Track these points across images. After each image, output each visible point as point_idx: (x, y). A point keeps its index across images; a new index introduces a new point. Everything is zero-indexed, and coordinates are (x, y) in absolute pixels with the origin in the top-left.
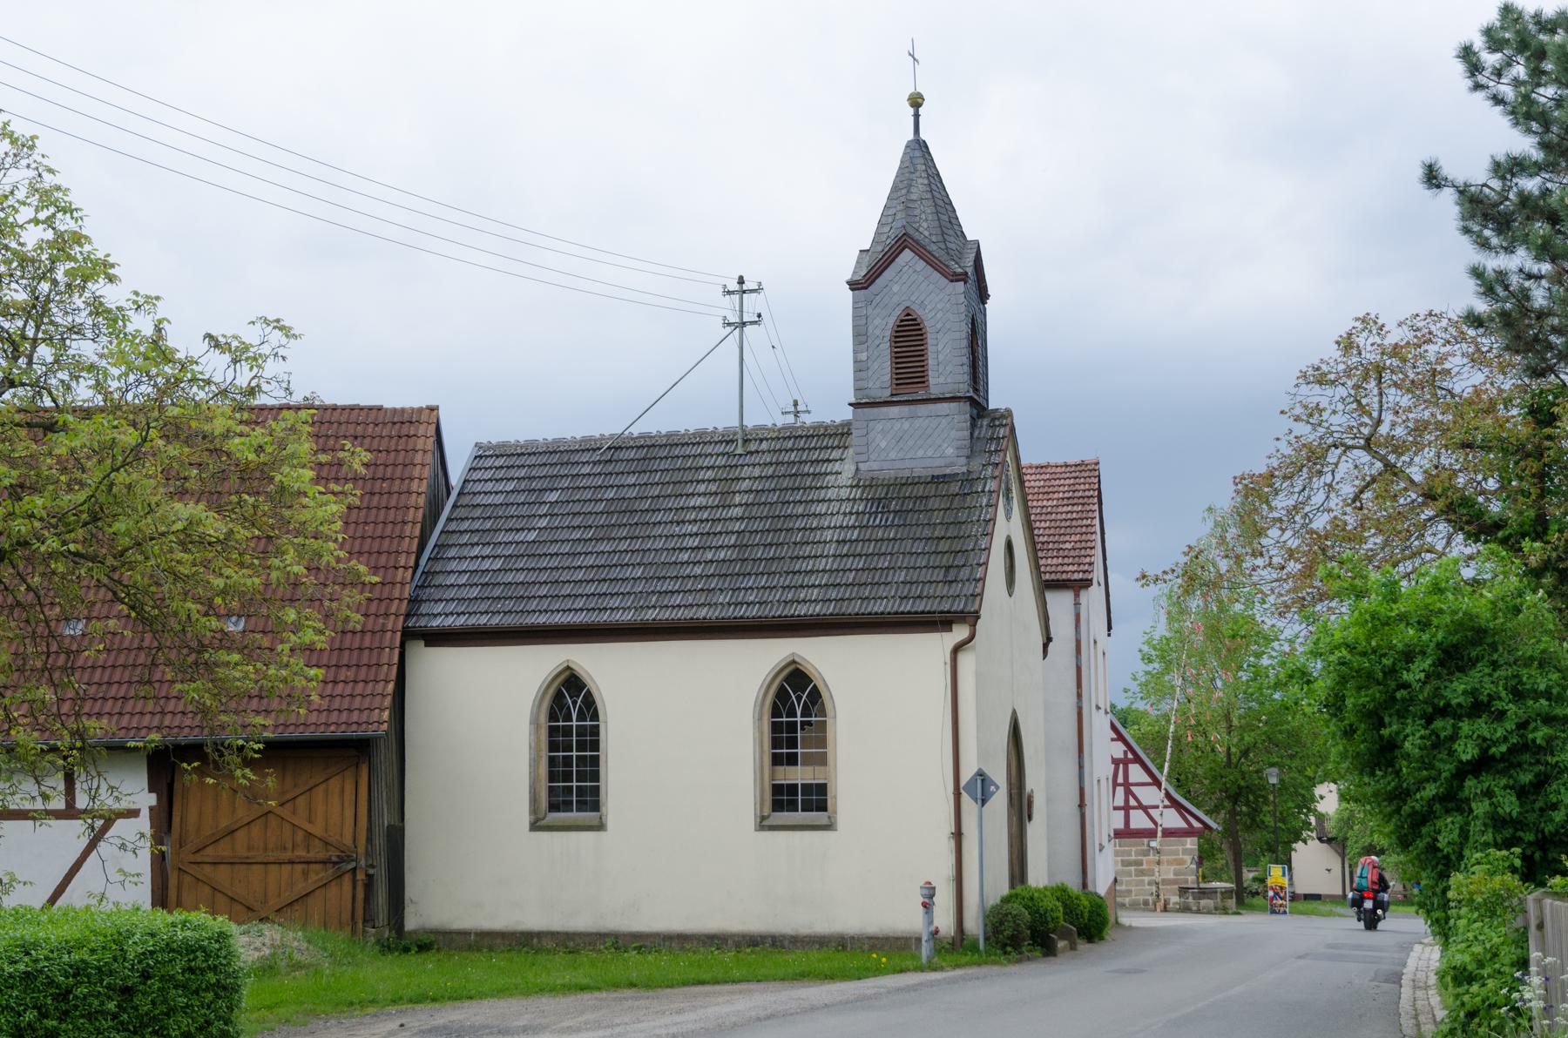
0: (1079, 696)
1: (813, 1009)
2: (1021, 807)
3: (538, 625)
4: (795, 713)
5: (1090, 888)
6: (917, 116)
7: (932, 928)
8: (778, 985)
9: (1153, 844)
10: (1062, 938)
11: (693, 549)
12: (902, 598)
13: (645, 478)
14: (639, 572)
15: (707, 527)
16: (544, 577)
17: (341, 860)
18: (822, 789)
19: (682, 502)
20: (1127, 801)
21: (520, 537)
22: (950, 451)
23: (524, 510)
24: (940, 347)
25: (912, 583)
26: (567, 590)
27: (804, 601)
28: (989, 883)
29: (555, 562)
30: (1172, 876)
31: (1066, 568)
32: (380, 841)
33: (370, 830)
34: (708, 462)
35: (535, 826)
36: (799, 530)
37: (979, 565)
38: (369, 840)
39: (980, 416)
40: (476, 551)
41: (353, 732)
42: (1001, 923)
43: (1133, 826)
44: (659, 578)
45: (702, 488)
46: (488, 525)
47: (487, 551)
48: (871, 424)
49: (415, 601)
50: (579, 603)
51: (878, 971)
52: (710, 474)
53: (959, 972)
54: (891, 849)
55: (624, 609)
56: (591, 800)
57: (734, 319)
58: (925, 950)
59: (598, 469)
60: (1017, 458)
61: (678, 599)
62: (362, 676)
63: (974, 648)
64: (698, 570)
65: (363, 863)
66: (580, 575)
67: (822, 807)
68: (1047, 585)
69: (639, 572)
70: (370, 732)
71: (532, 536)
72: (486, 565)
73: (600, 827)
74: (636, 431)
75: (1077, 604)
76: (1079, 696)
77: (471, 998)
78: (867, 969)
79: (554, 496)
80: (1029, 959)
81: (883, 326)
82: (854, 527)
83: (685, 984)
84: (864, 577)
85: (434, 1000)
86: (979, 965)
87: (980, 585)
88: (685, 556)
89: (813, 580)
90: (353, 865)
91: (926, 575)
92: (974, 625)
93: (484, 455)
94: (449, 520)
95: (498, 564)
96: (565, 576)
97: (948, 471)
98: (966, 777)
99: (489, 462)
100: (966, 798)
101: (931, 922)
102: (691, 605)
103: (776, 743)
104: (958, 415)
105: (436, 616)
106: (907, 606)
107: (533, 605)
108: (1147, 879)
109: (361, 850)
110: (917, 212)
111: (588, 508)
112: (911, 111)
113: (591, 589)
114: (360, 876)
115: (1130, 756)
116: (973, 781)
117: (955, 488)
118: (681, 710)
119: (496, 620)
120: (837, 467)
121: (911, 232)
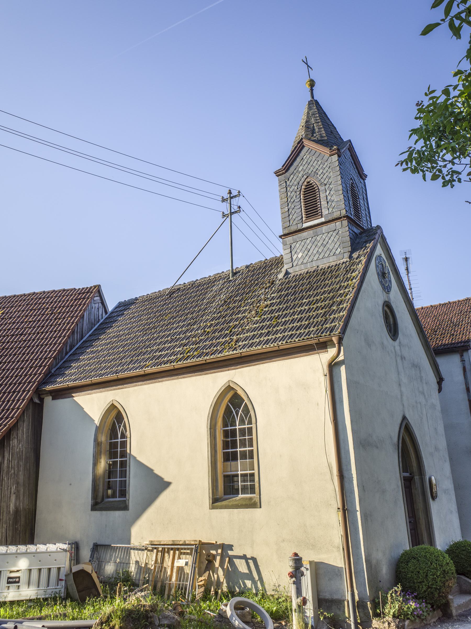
74: (187, 279)
104: (343, 228)
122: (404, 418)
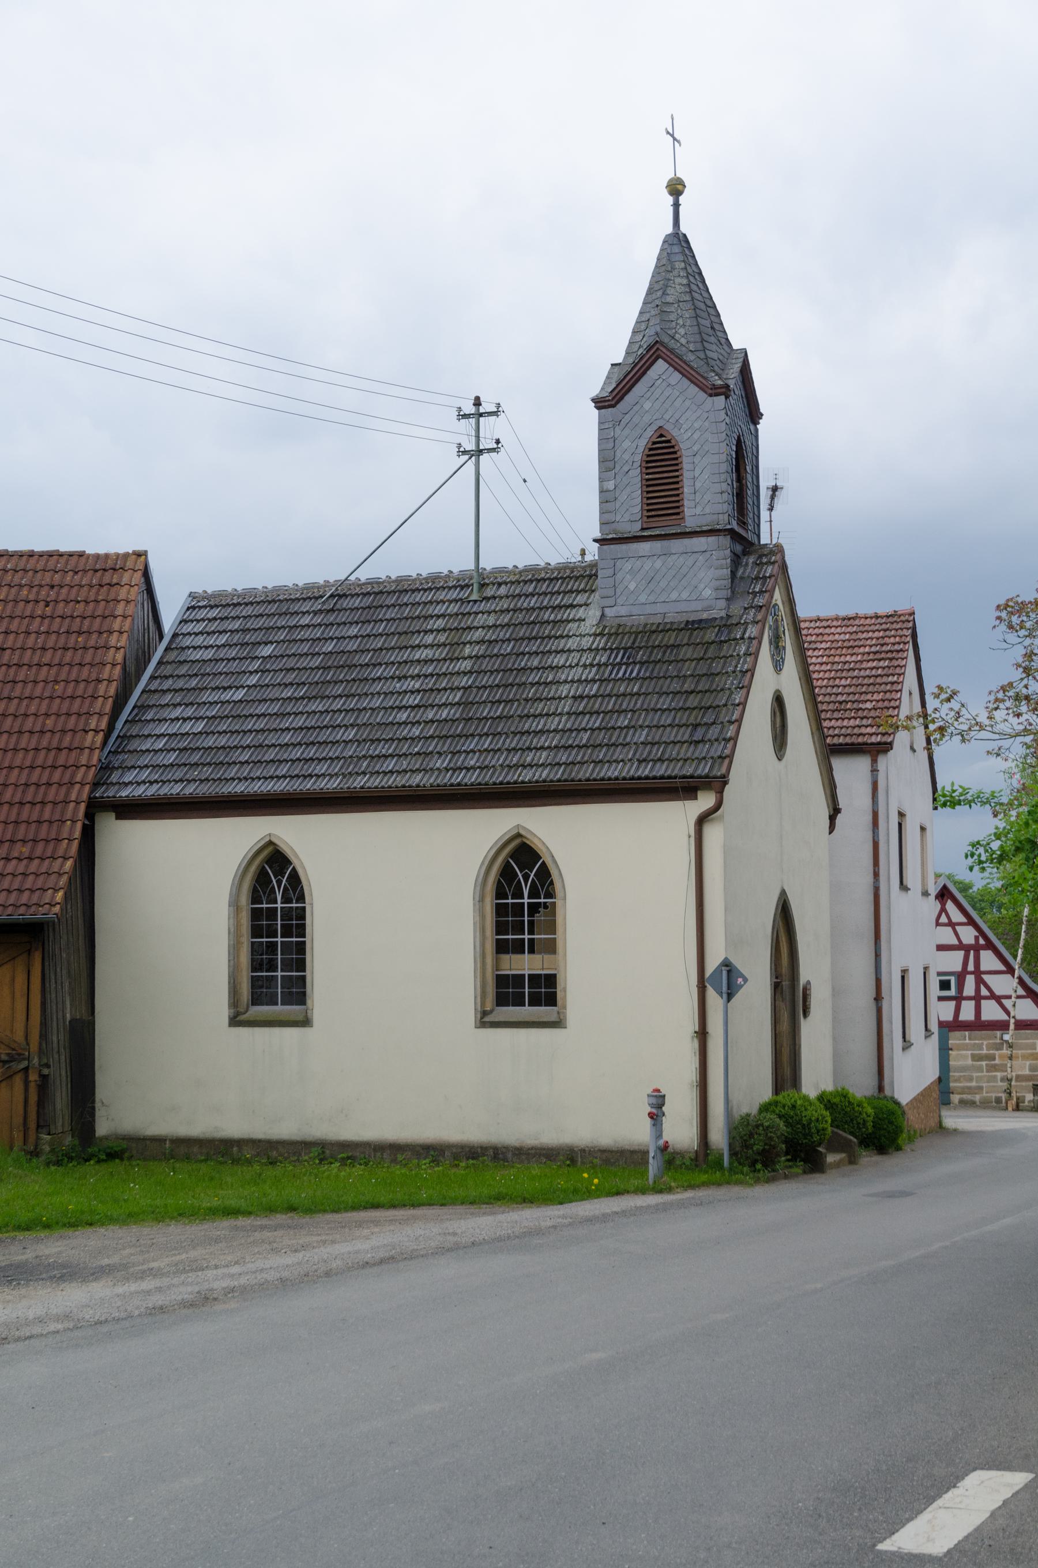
0: (876, 875)
1: (411, 1256)
2: (790, 997)
3: (236, 795)
4: (521, 897)
5: (887, 1092)
6: (676, 206)
7: (661, 1142)
8: (460, 1209)
9: (1006, 1037)
10: (832, 1148)
11: (413, 707)
12: (640, 762)
13: (368, 629)
14: (351, 734)
15: (430, 683)
16: (248, 740)
17: (12, 1059)
18: (551, 980)
19: (406, 655)
20: (978, 990)
21: (227, 696)
22: (708, 593)
23: (233, 666)
24: (697, 473)
25: (653, 744)
26: (271, 754)
27: (531, 766)
28: (747, 1083)
29: (261, 724)
30: (1027, 1072)
31: (863, 730)
32: (58, 1037)
33: (44, 1024)
34: (440, 609)
35: (236, 1021)
36: (532, 684)
37: (731, 722)
38: (44, 1036)
39: (745, 553)
40: (177, 712)
41: (21, 915)
42: (751, 1135)
43: (985, 1016)
44: (372, 741)
45: (429, 639)
46: (194, 683)
47: (189, 712)
48: (619, 563)
49: (106, 768)
50: (283, 770)
51: (586, 1194)
52: (440, 623)
53: (689, 1194)
54: (629, 1047)
55: (331, 776)
56: (297, 992)
57: (470, 446)
58: (653, 1167)
59: (318, 620)
60: (791, 602)
61: (390, 764)
62: (38, 851)
63: (722, 817)
64: (416, 731)
65: (36, 1061)
66: (287, 738)
67: (551, 1000)
68: (831, 751)
69: (351, 734)
70: (39, 914)
71: (240, 695)
72: (187, 727)
73: (305, 1022)
74: (364, 575)
75: (874, 771)
76: (876, 875)
77: (91, 1224)
78: (575, 1191)
79: (267, 651)
80: (786, 1177)
81: (633, 448)
82: (594, 681)
83: (355, 1208)
84: (600, 737)
85: (47, 1226)
86: (719, 1184)
87: (730, 745)
88: (403, 716)
89: (543, 741)
90: (25, 1064)
91: (670, 735)
92: (720, 792)
93: (198, 605)
94: (153, 678)
95: (200, 726)
96: (272, 739)
97: (705, 616)
98: (710, 968)
99: (202, 614)
100: (711, 993)
101: (659, 1135)
102: (405, 771)
103: (500, 928)
104: (718, 549)
105: (126, 784)
106: (646, 771)
107: (233, 772)
108: (999, 1075)
109: (34, 1046)
110: (672, 317)
111: (304, 663)
112: (670, 200)
113: (297, 753)
114: (33, 1077)
115: (982, 942)
116: (718, 971)
117: (710, 635)
118: (401, 891)
119: (190, 789)
120: (581, 613)
121: (666, 339)
122: (783, 893)
